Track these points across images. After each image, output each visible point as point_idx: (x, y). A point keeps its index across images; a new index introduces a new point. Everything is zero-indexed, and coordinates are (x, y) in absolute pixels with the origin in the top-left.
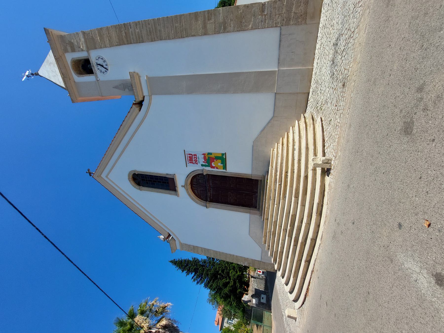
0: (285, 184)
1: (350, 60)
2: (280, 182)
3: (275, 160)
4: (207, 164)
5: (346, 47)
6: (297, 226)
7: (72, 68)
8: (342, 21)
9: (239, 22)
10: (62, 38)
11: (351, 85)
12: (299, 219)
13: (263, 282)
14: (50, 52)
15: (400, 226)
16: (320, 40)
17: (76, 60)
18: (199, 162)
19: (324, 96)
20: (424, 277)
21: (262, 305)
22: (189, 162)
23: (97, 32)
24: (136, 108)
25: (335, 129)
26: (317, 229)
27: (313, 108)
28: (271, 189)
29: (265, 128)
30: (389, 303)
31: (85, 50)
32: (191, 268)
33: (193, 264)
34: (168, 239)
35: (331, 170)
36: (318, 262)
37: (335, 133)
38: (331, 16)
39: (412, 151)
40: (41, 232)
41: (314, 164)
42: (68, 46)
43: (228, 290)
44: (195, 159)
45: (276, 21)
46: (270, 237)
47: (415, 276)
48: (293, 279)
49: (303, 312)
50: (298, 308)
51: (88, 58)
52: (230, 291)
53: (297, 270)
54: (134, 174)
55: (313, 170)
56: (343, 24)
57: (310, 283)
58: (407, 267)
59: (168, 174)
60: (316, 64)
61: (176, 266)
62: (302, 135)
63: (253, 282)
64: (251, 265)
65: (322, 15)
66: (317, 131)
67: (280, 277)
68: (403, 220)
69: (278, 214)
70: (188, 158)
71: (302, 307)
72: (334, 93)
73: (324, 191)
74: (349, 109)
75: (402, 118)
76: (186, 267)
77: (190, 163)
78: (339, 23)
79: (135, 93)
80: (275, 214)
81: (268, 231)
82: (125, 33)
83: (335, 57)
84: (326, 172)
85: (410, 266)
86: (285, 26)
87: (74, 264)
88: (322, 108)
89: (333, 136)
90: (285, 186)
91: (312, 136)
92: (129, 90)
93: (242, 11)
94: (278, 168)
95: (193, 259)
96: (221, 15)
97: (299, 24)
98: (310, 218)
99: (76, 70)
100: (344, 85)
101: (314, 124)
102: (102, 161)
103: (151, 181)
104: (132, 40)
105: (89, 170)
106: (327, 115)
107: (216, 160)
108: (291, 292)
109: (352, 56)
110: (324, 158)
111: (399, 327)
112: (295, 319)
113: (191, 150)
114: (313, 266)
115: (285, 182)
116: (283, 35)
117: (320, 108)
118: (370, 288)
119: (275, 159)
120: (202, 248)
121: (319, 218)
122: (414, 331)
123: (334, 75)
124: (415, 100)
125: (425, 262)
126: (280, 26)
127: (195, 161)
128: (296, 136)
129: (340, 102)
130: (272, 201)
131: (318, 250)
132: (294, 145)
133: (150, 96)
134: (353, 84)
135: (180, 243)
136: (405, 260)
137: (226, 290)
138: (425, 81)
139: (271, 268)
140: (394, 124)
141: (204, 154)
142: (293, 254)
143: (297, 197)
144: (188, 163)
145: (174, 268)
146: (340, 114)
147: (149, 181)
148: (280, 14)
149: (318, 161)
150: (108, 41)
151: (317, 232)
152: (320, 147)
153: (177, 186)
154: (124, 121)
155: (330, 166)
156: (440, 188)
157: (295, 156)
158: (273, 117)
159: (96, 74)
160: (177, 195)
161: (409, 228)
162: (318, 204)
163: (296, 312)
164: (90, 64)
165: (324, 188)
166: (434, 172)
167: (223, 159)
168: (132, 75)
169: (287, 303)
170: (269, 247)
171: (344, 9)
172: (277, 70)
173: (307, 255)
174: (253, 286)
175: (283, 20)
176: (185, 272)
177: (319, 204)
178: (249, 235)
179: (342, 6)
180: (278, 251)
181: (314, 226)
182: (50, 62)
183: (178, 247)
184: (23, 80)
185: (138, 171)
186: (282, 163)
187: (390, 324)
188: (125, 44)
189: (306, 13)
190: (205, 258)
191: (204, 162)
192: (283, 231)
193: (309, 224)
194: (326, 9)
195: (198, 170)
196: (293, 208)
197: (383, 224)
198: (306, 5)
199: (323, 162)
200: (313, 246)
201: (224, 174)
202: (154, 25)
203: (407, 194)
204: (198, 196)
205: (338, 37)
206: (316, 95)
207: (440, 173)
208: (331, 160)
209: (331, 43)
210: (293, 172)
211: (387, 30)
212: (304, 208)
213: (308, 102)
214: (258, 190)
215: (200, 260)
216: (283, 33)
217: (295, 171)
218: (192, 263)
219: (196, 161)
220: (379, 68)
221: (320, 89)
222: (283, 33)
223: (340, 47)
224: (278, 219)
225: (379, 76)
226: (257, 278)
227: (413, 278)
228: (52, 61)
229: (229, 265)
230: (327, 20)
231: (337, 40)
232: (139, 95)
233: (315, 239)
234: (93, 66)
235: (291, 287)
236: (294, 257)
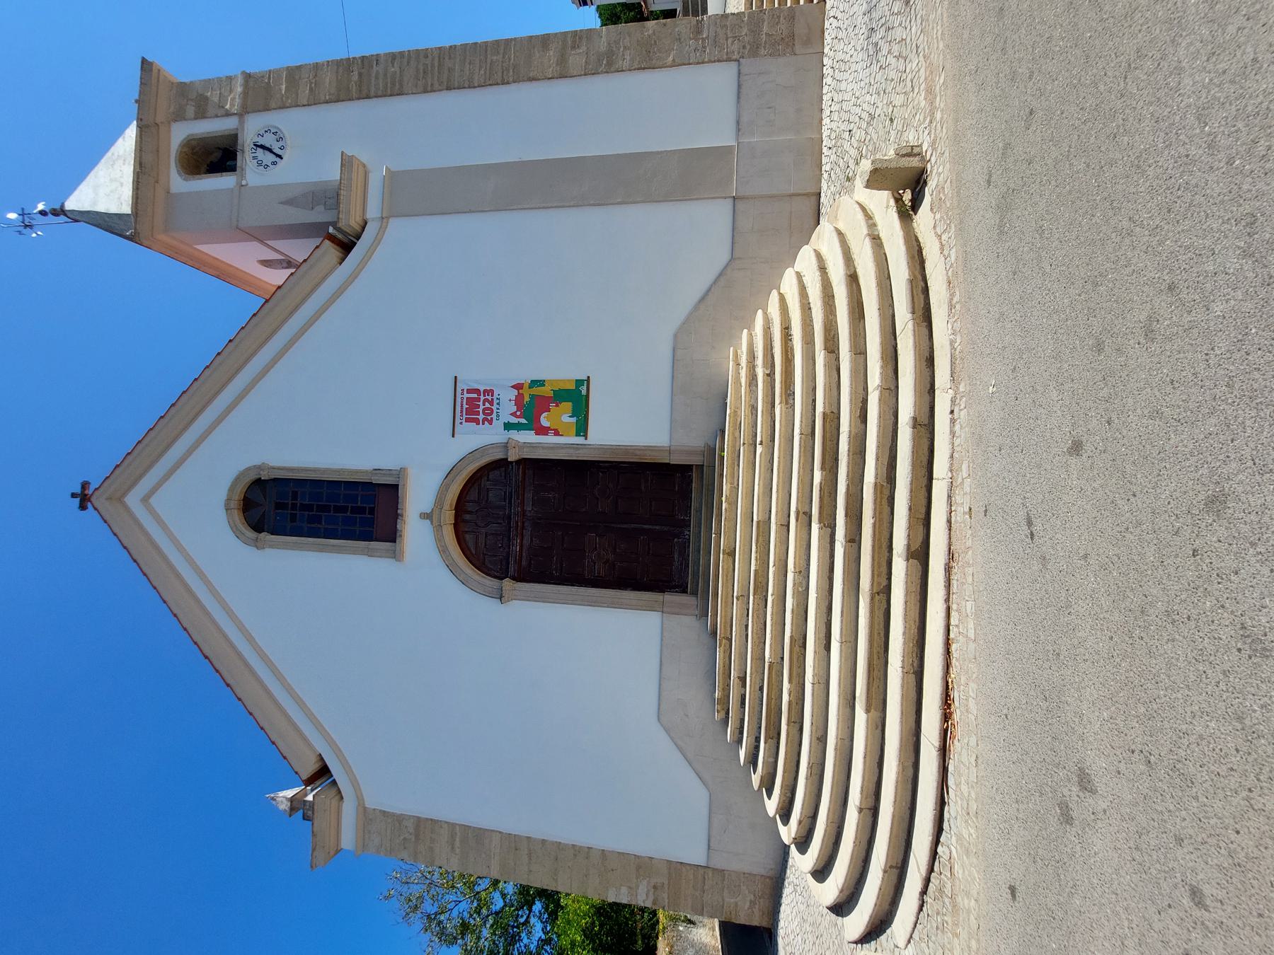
4: (523, 421)
18: (498, 416)
23: (285, 73)
26: (927, 372)
28: (739, 420)
29: (709, 290)
34: (312, 785)
44: (487, 405)
45: (727, 48)
53: (875, 657)
54: (258, 484)
64: (665, 896)
69: (771, 489)
77: (466, 422)
81: (735, 594)
82: (360, 75)
86: (749, 58)
90: (786, 363)
92: (325, 208)
93: (651, 32)
96: (604, 39)
107: (557, 406)
113: (474, 377)
115: (786, 351)
116: (746, 75)
121: (926, 332)
126: (738, 58)
127: (484, 413)
130: (744, 451)
139: (751, 901)
141: (518, 387)
143: (832, 347)
144: (461, 423)
148: (736, 37)
150: (307, 92)
151: (928, 388)
153: (402, 516)
158: (732, 259)
160: (396, 556)
172: (734, 143)
173: (910, 509)
175: (744, 47)
189: (792, 36)
191: (514, 414)
192: (797, 520)
199: (898, 154)
202: (439, 58)
214: (690, 516)
216: (745, 70)
219: (487, 412)
224: (770, 511)
232: (352, 212)
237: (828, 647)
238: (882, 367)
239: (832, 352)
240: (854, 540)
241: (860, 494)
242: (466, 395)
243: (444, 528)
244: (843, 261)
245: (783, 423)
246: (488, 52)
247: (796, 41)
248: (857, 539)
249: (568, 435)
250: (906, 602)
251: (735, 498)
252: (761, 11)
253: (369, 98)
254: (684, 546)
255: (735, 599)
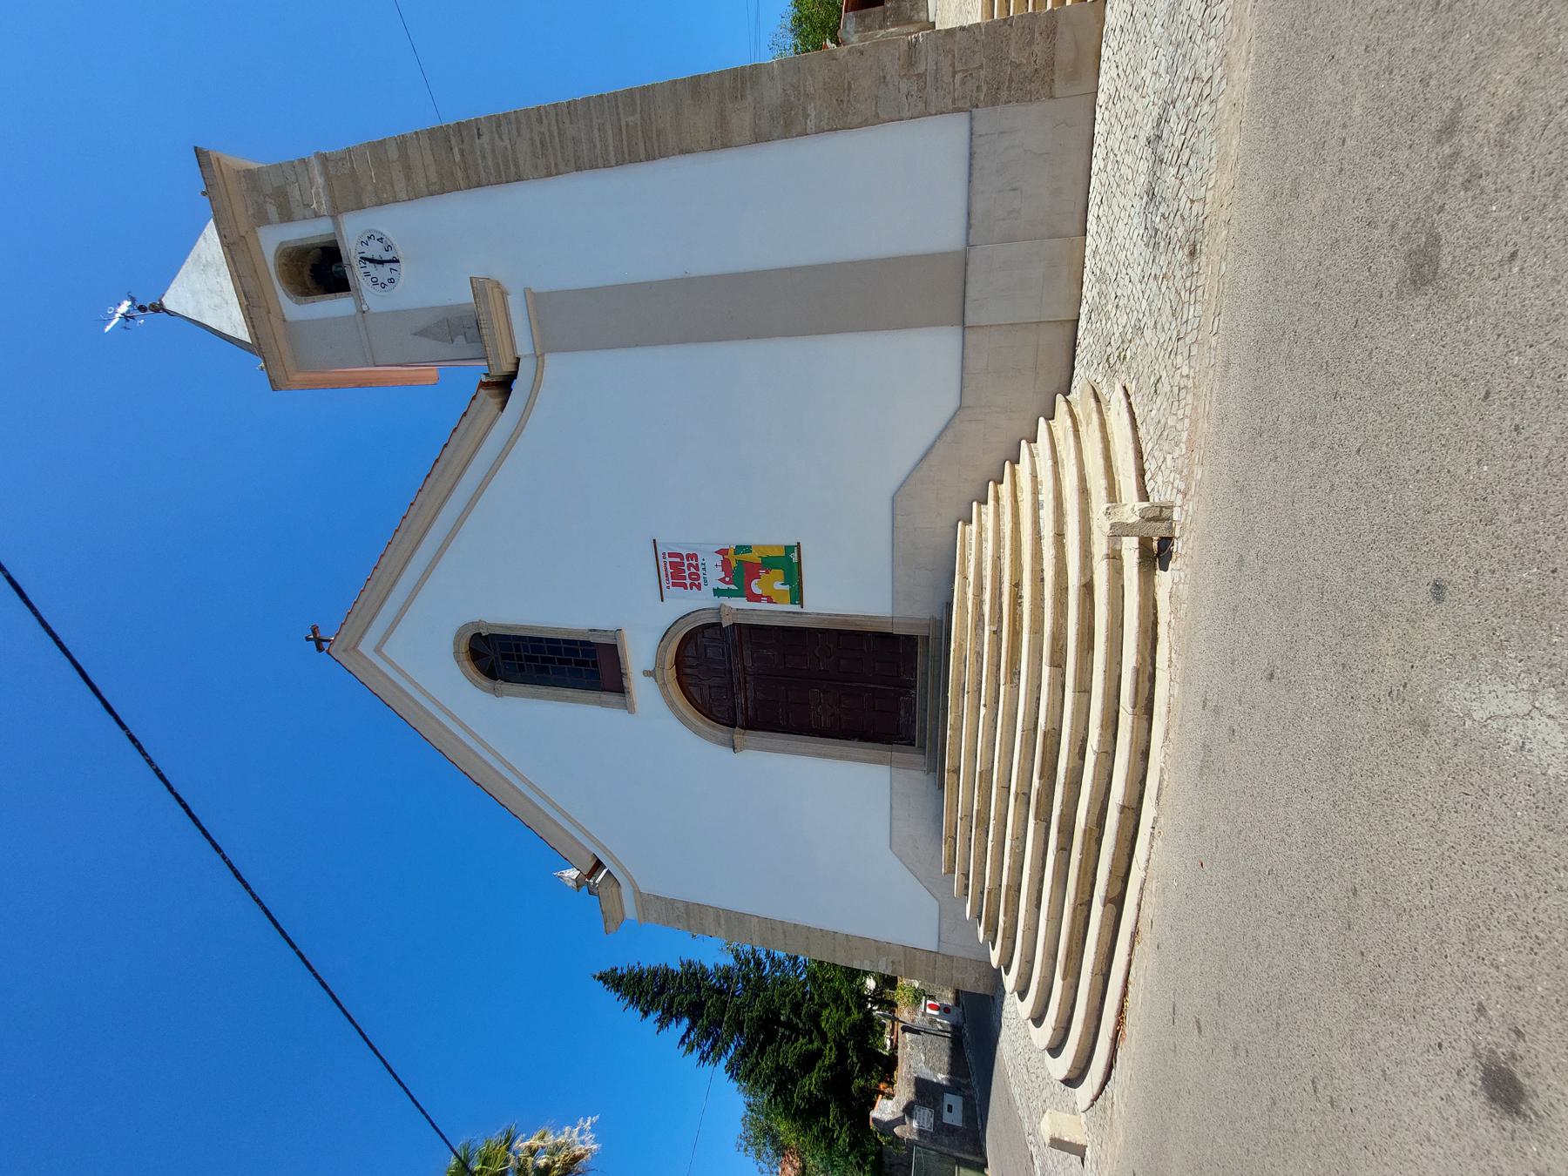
0: (1014, 625)
1: (1206, 166)
2: (994, 625)
3: (973, 554)
4: (733, 587)
5: (1189, 133)
6: (1067, 768)
7: (276, 273)
8: (1171, 62)
9: (835, 101)
10: (251, 178)
11: (1215, 244)
12: (1070, 741)
13: (945, 1044)
14: (208, 226)
15: (1438, 590)
16: (1102, 144)
17: (293, 248)
19: (1128, 314)
20: (1550, 716)
21: (947, 1136)
22: (671, 581)
24: (489, 400)
25: (1176, 403)
27: (1095, 365)
28: (947, 845)
29: (932, 446)
30: (1433, 884)
31: (326, 213)
32: (677, 1000)
33: (684, 985)
34: (594, 878)
35: (1173, 545)
36: (1154, 890)
37: (1176, 415)
38: (1132, 62)
39: (1445, 327)
40: (144, 754)
41: (1113, 526)
42: (271, 203)
43: (816, 1083)
44: (693, 570)
46: (970, 839)
47: (1514, 735)
48: (1063, 985)
49: (1109, 1112)
50: (1088, 1103)
51: (332, 238)
52: (826, 1085)
53: (1074, 946)
54: (477, 636)
55: (1108, 557)
56: (1175, 68)
57: (1127, 986)
58: (1485, 718)
59: (595, 630)
60: (1095, 221)
61: (618, 994)
62: (1064, 456)
63: (912, 1048)
64: (903, 969)
65: (1104, 66)
66: (1112, 433)
67: (1012, 993)
68: (1446, 566)
70: (666, 570)
71: (1104, 1093)
72: (1164, 289)
73: (1155, 623)
74: (1217, 318)
75: (1398, 246)
76: (656, 997)
77: (673, 586)
78: (1162, 71)
79: (488, 348)
80: (984, 743)
81: (959, 815)
82: (462, 152)
83: (1156, 178)
84: (1156, 555)
85: (1493, 709)
87: (253, 895)
88: (1125, 355)
89: (1171, 427)
90: (1013, 635)
91: (1099, 447)
94: (986, 576)
95: (682, 965)
97: (1030, 100)
98: (1110, 732)
99: (291, 284)
100: (1192, 253)
101: (1100, 412)
102: (362, 591)
103: (535, 659)
104: (483, 175)
105: (314, 630)
106: (1146, 371)
107: (767, 573)
108: (1055, 1050)
109: (1213, 154)
110: (1146, 504)
111: (1481, 954)
112: (1079, 1151)
113: (677, 539)
114: (1136, 910)
115: (1015, 621)
116: (980, 136)
117: (1119, 357)
118: (1358, 871)
119: (973, 552)
120: (717, 908)
121: (1145, 724)
122: (1538, 934)
123: (1156, 234)
124: (1436, 169)
125: (1545, 662)
128: (1042, 463)
129: (1184, 309)
131: (1150, 843)
132: (1036, 492)
133: (539, 358)
134: (1225, 233)
135: (637, 891)
136: (1474, 697)
137: (810, 1083)
138: (1459, 99)
139: (976, 978)
140: (1374, 280)
141: (722, 552)
142: (1057, 883)
143: (1058, 663)
144: (668, 587)
145: (611, 1002)
146: (1188, 347)
147: (528, 659)
148: (967, 71)
149: (1125, 516)
152: (1130, 478)
153: (626, 675)
154: (446, 445)
155: (1171, 529)
156: (1558, 391)
157: (1042, 525)
158: (960, 407)
159: (357, 290)
160: (629, 707)
161: (1471, 581)
162: (1137, 671)
163: (1083, 1123)
164: (341, 261)
165: (1155, 614)
166: (1530, 352)
167: (789, 564)
168: (479, 287)
169: (1045, 1101)
170: (968, 880)
171: (1174, 24)
173: (1111, 872)
174: (912, 1063)
175: (979, 88)
176: (654, 1016)
177: (1141, 670)
178: (891, 848)
179: (1166, 18)
180: (1001, 886)
181: (1127, 757)
182: (207, 261)
183: (631, 911)
184: (108, 328)
185: (491, 625)
186: (999, 558)
187: (1449, 959)
188: (458, 190)
189: (1051, 64)
190: (729, 961)
191: (722, 580)
192: (1016, 801)
193: (1108, 753)
194: (1114, 44)
195: (704, 609)
196: (1048, 705)
197: (1376, 619)
198: (1048, 38)
199: (1143, 518)
200: (1129, 837)
201: (795, 620)
203: (1449, 472)
204: (704, 711)
205: (1161, 113)
206: (1101, 321)
207: (1551, 344)
208: (1171, 508)
209: (1140, 138)
210: (1038, 579)
211: (1317, 22)
212: (1086, 698)
213: (1075, 351)
214: (916, 677)
215: (710, 966)
217: (1045, 576)
218: (680, 983)
219: (695, 577)
220: (1303, 141)
221: (1113, 296)
222: (978, 129)
223: (1171, 141)
224: (993, 762)
225: (1309, 162)
226: (925, 1032)
227: (1512, 743)
228: (213, 255)
229: (820, 987)
230: (1122, 75)
231: (1158, 125)
233: (1134, 806)
234: (350, 265)
235: (1056, 1021)
236: (1060, 896)
237: (1038, 906)
238: (1101, 735)
239: (1059, 666)
240: (1065, 848)
241: (1073, 816)
242: (669, 560)
243: (669, 686)
244: (1078, 537)
245: (1007, 703)
246: (620, 109)
247: (1057, 75)
248: (1068, 848)
249: (782, 603)
250: (1099, 934)
251: (960, 725)
252: (1005, 20)
253: (482, 186)
254: (911, 705)
255: (959, 820)
